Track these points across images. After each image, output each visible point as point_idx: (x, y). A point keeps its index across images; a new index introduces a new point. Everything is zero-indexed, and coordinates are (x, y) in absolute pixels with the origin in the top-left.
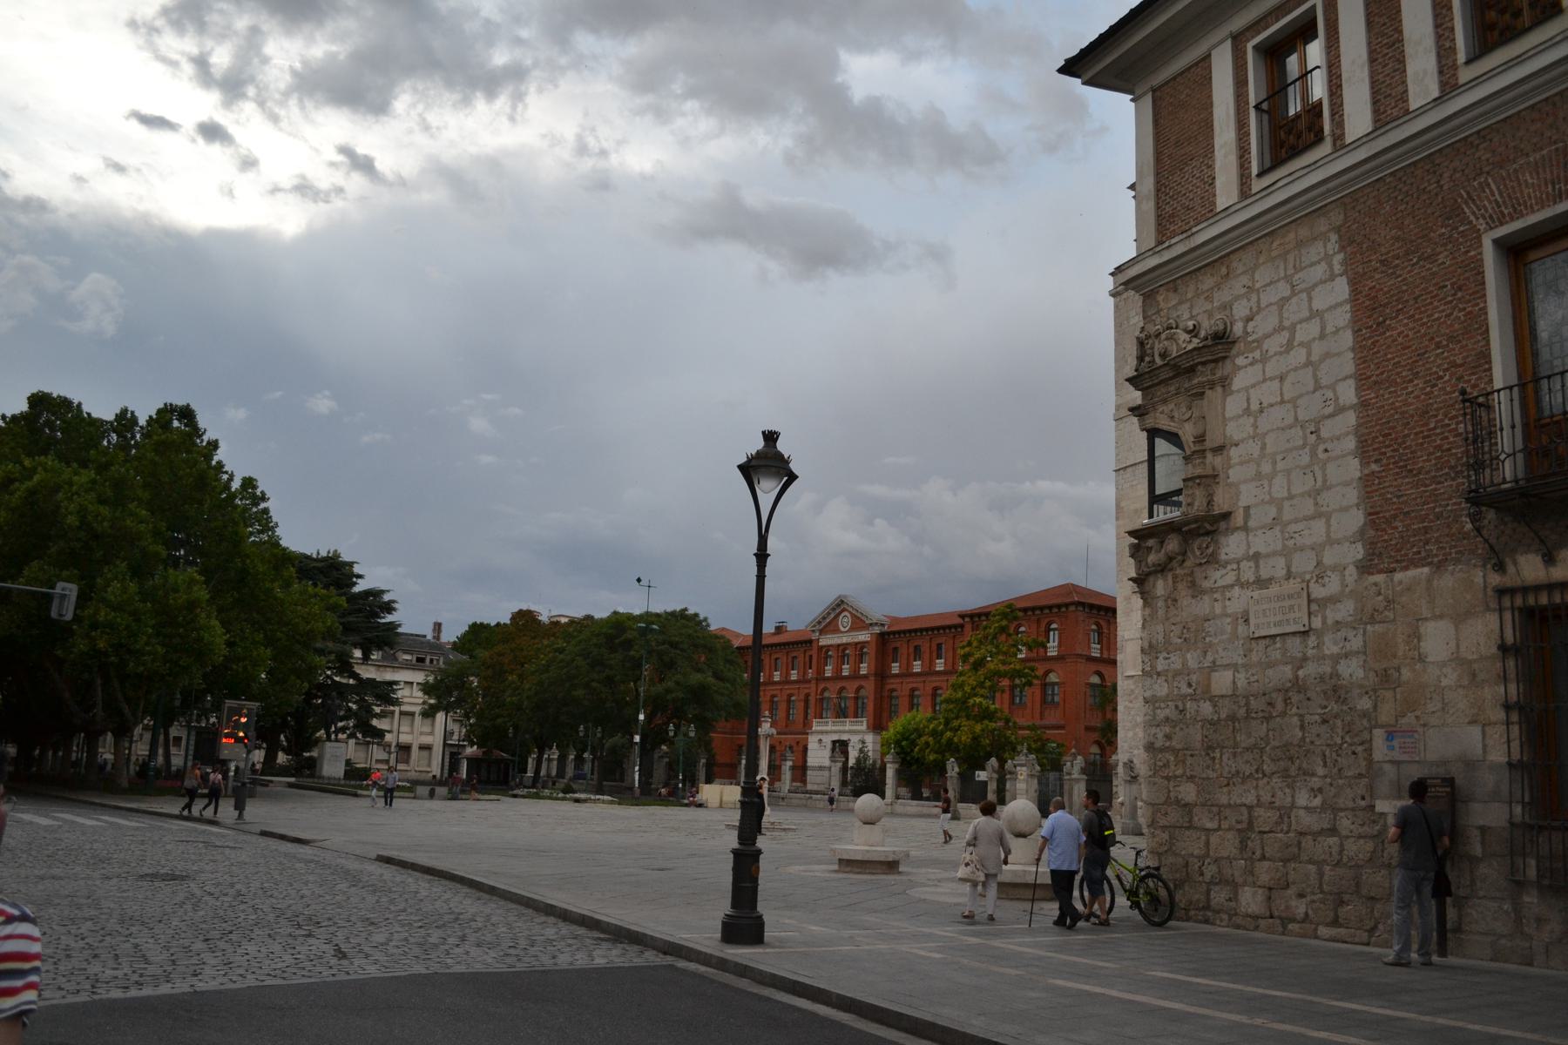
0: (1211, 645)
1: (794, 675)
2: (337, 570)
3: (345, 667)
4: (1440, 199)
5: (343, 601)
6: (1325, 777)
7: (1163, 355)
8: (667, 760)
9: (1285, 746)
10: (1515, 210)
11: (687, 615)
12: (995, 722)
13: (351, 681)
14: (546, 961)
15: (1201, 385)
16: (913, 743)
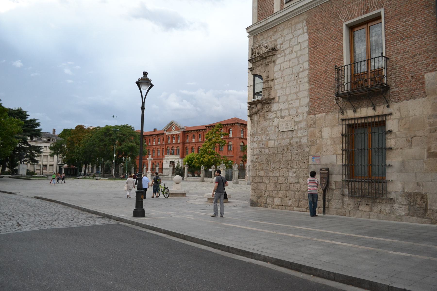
0: (268, 134)
1: (159, 143)
2: (21, 113)
3: (25, 142)
4: (333, 12)
5: (23, 122)
6: (297, 169)
7: (258, 54)
8: (123, 167)
9: (287, 161)
10: (352, 16)
11: (128, 126)
12: (215, 155)
13: (28, 147)
14: (81, 224)
15: (268, 62)
16: (192, 162)
